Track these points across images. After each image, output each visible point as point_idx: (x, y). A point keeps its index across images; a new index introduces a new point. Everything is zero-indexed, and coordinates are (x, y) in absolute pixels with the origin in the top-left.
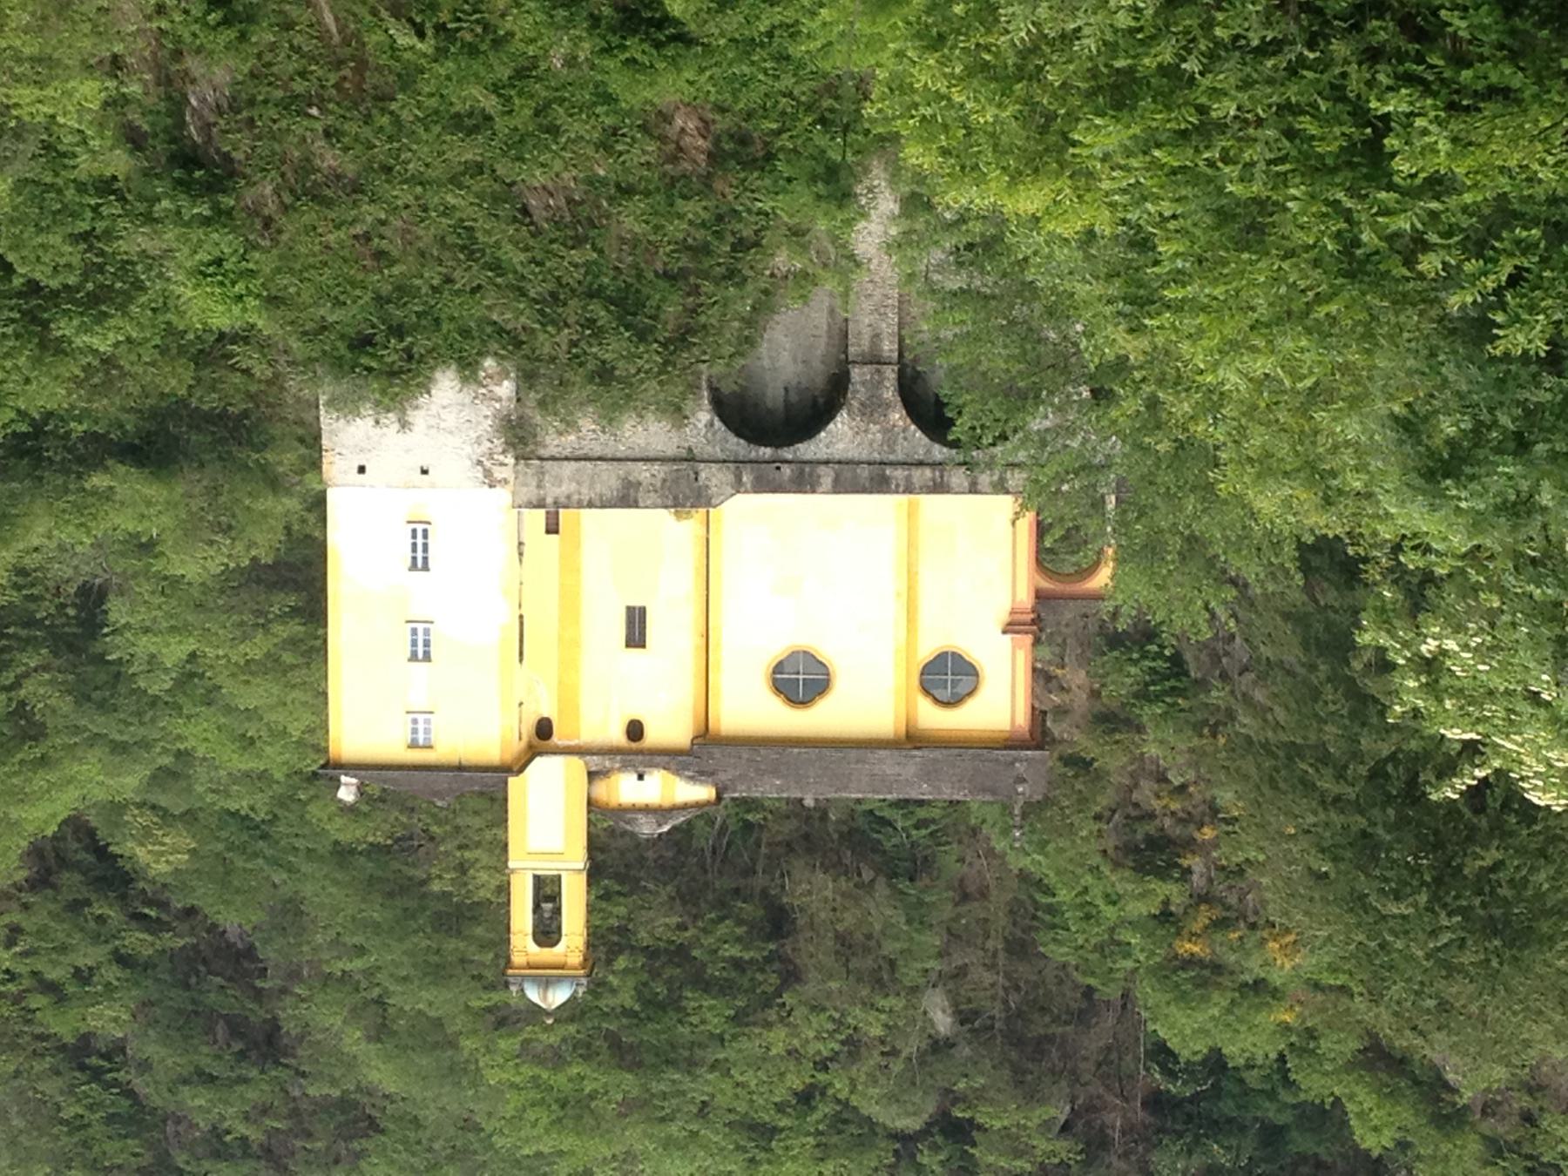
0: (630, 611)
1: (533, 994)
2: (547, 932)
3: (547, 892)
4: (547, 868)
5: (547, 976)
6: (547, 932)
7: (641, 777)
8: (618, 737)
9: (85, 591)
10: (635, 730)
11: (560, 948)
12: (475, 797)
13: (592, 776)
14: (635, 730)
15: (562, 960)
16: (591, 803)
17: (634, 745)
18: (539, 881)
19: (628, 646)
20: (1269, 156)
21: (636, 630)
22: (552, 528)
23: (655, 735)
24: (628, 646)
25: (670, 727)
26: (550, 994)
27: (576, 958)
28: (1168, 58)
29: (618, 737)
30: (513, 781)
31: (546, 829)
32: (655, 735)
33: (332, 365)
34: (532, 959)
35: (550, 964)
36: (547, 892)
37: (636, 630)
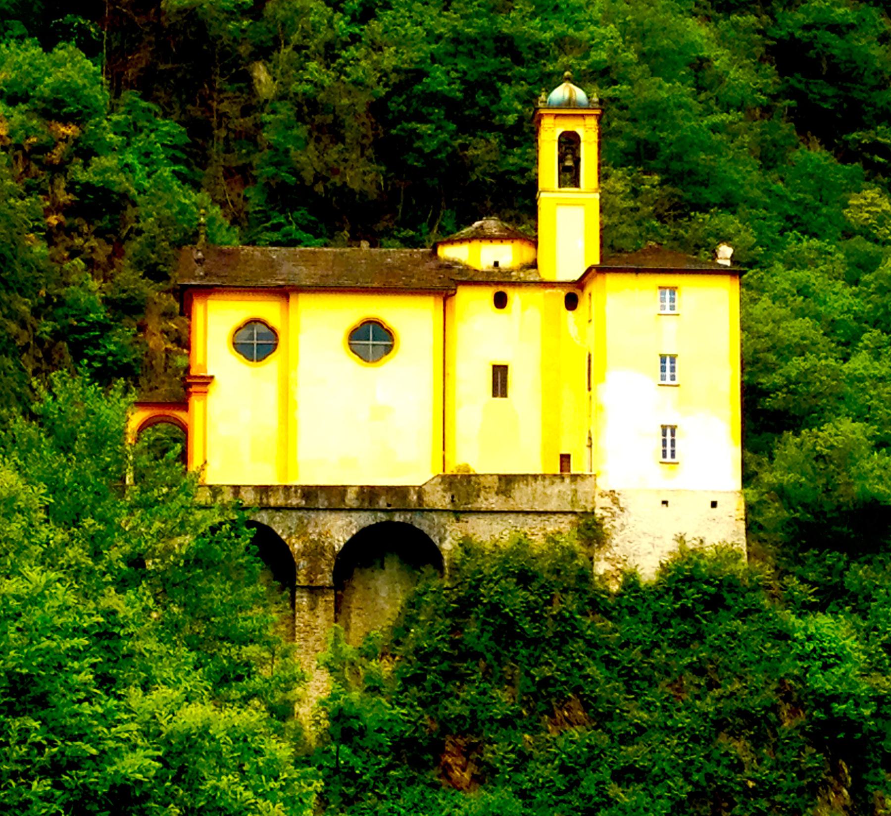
2: (569, 144)
3: (569, 175)
4: (569, 192)
6: (569, 144)
7: (496, 264)
8: (514, 296)
10: (500, 301)
11: (559, 130)
12: (653, 235)
13: (534, 265)
14: (500, 301)
15: (559, 121)
21: (500, 379)
23: (487, 295)
25: (473, 302)
27: (547, 122)
29: (514, 296)
34: (580, 121)
36: (569, 175)
37: (500, 379)
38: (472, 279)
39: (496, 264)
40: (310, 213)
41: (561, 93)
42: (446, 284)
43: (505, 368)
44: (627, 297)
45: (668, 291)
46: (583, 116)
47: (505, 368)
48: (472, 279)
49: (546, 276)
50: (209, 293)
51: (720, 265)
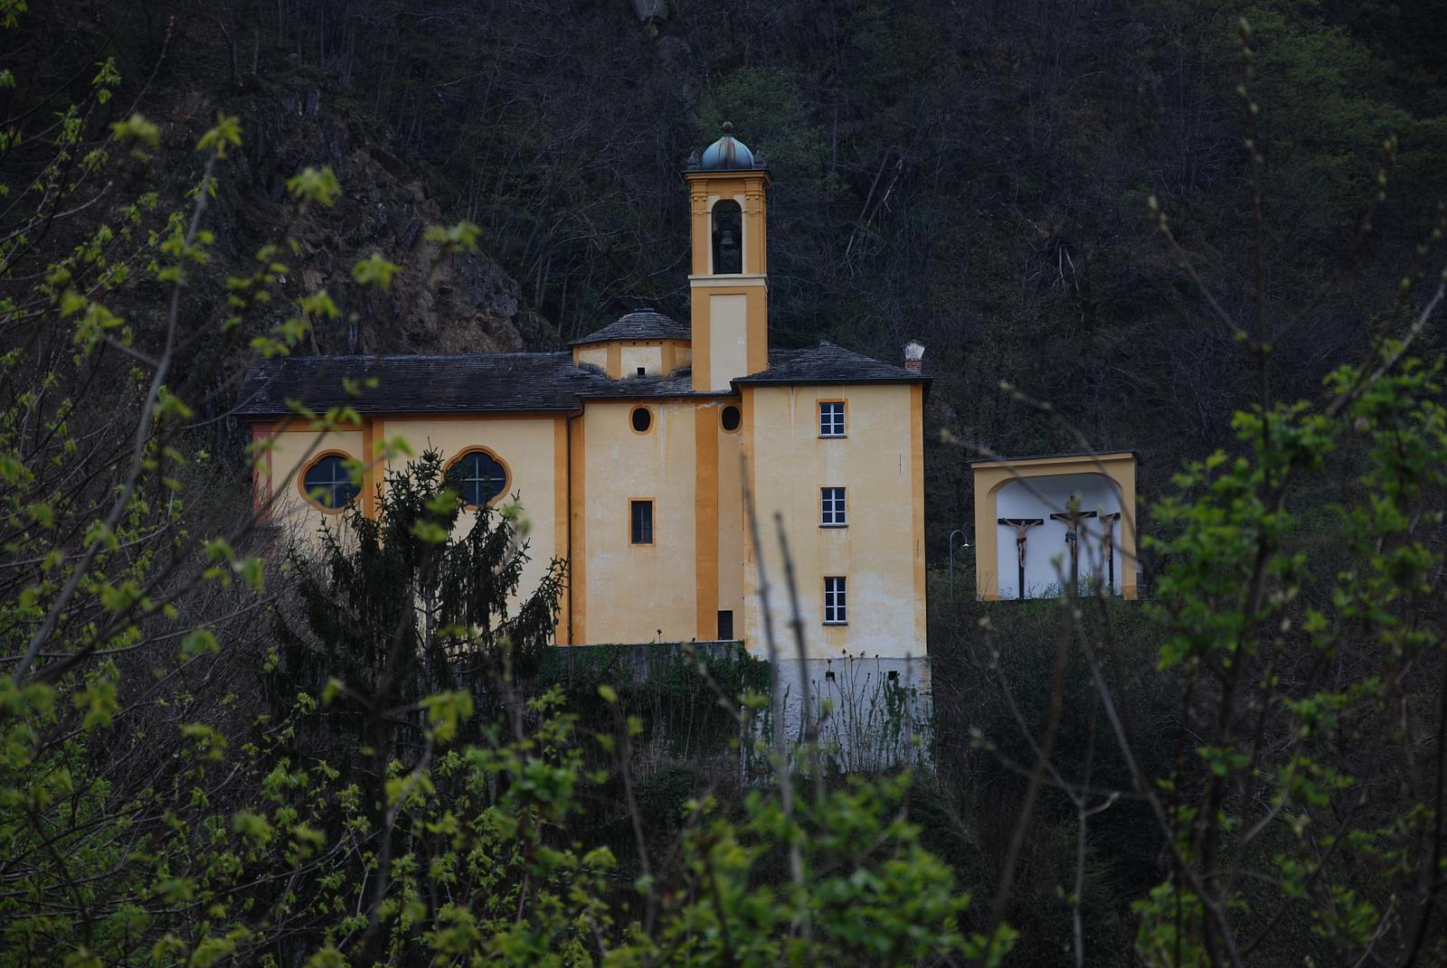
0: (649, 540)
1: (741, 149)
2: (727, 217)
3: (727, 260)
4: (728, 280)
5: (728, 169)
6: (727, 217)
7: (641, 371)
8: (660, 415)
9: (1165, 556)
10: (641, 422)
11: (713, 200)
12: (813, 342)
13: (686, 373)
14: (641, 422)
15: (712, 188)
16: (687, 343)
17: (644, 406)
18: (736, 268)
19: (650, 503)
20: (14, 829)
21: (642, 516)
22: (725, 619)
23: (621, 417)
24: (650, 503)
25: (607, 425)
26: (724, 152)
27: (698, 190)
28: (1032, 704)
29: (660, 415)
30: (762, 366)
31: (730, 326)
32: (621, 417)
33: (773, 835)
34: (740, 187)
35: (729, 184)
36: (727, 260)
37: (642, 516)
38: (611, 393)
39: (641, 371)
40: (418, 941)
41: (715, 150)
42: (567, 404)
43: (841, 492)
44: (781, 421)
45: (159, 586)
46: (742, 180)
47: (841, 492)
48: (611, 393)
49: (698, 387)
50: (273, 423)
51: (908, 373)
